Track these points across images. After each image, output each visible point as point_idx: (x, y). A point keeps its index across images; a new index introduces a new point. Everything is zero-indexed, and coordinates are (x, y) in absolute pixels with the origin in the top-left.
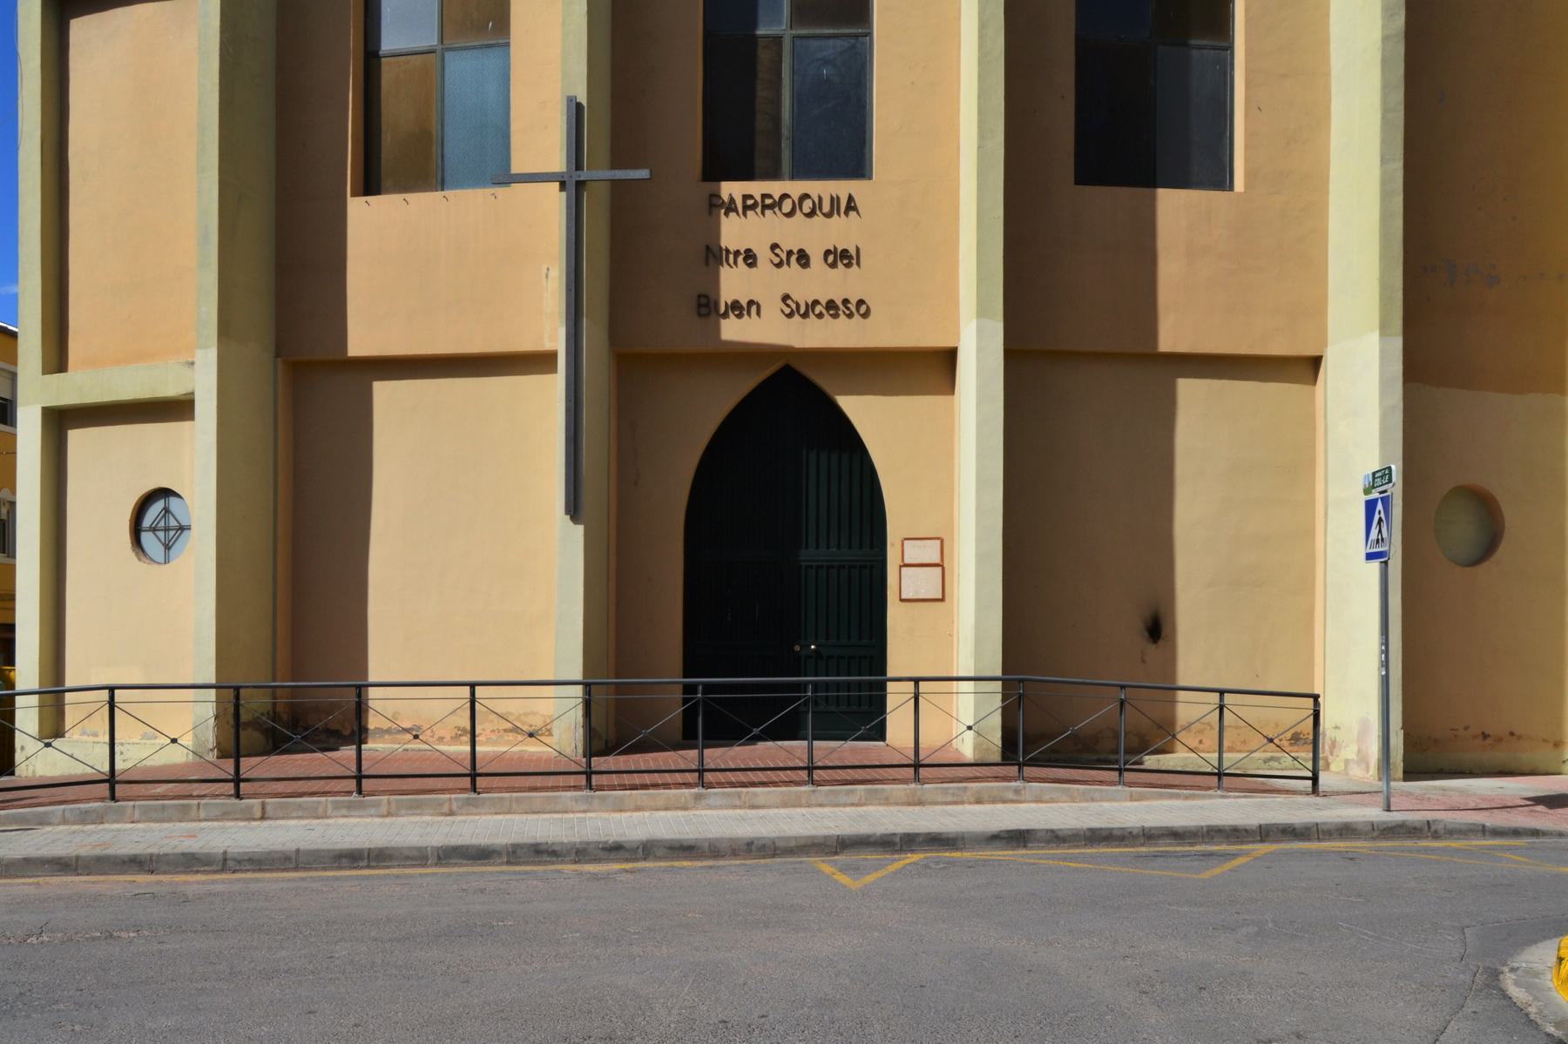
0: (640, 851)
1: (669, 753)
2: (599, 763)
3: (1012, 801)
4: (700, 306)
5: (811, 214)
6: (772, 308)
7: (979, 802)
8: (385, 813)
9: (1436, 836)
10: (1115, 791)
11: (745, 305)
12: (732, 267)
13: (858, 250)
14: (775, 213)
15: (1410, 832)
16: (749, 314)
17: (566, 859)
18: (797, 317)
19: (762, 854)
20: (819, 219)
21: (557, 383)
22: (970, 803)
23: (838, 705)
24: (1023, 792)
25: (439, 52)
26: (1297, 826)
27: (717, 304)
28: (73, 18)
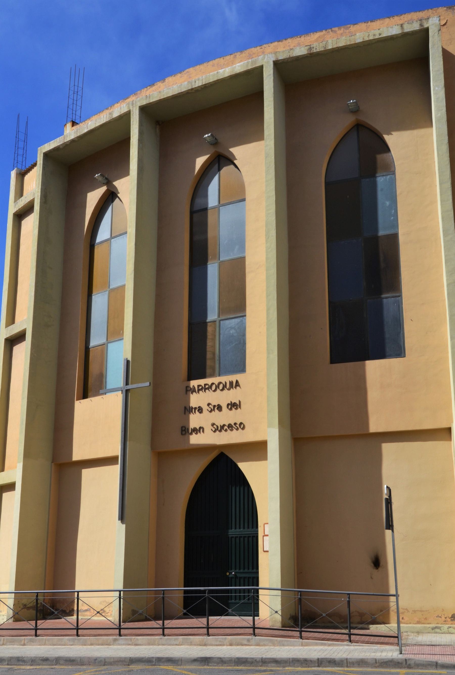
0: (54, 661)
1: (152, 622)
2: (123, 625)
3: (246, 645)
4: (182, 431)
5: (222, 390)
6: (208, 429)
7: (231, 645)
8: (2, 644)
9: (409, 667)
10: (294, 641)
11: (198, 429)
12: (194, 414)
13: (240, 402)
14: (209, 391)
15: (395, 665)
16: (200, 432)
17: (28, 664)
18: (217, 432)
19: (100, 664)
20: (226, 391)
21: (116, 469)
22: (227, 645)
23: (236, 600)
24: (251, 641)
25: (106, 344)
26: (336, 660)
27: (188, 429)
28: (14, 346)
